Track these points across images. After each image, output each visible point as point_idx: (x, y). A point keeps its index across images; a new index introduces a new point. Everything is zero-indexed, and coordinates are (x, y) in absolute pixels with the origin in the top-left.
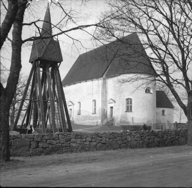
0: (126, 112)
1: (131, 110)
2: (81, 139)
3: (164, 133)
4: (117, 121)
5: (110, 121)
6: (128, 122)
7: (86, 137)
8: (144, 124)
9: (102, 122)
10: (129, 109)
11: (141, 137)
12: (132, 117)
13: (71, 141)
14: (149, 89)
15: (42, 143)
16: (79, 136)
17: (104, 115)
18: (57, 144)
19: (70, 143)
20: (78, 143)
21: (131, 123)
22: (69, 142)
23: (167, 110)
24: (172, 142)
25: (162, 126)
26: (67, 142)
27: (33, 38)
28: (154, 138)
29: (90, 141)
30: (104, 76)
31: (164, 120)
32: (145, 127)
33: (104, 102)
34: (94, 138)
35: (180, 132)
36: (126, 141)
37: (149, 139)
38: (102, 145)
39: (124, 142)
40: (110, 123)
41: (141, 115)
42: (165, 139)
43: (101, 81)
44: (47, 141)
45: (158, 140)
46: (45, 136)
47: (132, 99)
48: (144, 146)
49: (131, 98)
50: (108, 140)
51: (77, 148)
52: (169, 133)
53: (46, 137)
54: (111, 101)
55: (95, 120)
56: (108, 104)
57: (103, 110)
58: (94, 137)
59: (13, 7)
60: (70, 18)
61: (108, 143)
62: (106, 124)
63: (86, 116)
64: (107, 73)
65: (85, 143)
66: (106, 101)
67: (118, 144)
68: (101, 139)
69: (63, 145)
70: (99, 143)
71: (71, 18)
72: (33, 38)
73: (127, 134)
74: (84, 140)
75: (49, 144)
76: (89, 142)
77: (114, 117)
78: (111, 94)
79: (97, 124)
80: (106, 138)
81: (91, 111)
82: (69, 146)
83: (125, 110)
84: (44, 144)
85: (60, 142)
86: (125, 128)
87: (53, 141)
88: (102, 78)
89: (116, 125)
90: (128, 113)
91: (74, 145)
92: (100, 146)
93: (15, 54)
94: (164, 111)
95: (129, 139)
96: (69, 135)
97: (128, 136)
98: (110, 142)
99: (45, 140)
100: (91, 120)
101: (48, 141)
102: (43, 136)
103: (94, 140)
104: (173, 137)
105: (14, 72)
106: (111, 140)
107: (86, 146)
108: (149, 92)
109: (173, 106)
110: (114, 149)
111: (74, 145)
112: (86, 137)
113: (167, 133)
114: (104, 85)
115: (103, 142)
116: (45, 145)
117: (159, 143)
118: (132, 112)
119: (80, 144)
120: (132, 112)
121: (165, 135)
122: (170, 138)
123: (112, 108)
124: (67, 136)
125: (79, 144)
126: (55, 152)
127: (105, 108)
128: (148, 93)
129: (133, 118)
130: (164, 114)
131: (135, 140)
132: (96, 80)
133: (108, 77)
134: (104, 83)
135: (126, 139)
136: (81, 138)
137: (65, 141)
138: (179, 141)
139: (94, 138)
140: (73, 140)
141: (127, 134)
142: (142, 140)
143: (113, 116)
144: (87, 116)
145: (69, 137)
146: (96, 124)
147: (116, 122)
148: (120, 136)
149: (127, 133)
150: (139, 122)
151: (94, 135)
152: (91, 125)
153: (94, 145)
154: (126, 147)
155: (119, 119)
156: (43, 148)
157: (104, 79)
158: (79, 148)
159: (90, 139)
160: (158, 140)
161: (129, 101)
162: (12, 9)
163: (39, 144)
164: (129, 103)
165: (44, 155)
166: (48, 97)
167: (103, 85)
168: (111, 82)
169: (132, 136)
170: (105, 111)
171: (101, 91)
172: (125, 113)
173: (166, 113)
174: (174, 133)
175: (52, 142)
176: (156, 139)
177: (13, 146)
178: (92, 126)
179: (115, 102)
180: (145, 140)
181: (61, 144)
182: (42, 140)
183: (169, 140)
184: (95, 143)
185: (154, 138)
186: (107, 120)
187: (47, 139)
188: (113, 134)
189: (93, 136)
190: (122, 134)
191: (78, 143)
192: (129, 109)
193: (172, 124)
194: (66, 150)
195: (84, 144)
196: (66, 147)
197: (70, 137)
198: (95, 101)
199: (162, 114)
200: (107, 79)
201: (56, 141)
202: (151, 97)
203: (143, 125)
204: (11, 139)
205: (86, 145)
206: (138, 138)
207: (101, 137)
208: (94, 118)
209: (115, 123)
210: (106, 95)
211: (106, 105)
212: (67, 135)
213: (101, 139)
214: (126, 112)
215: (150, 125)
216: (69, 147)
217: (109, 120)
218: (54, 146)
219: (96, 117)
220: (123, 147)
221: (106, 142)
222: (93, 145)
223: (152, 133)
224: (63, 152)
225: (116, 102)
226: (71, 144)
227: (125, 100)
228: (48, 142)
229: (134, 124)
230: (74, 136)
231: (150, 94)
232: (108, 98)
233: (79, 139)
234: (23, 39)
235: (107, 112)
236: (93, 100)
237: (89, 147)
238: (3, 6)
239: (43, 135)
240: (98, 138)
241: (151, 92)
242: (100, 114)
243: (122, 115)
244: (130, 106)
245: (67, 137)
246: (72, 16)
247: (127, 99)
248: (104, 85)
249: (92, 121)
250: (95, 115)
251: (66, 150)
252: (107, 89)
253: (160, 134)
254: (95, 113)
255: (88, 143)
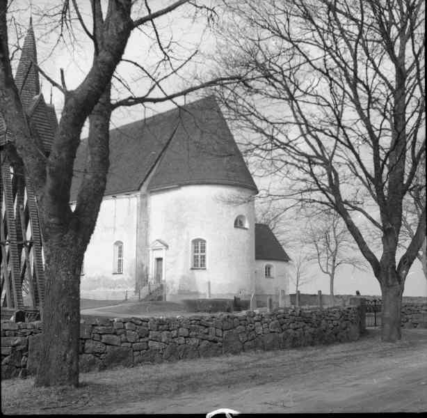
0: (192, 269)
1: (203, 265)
2: (168, 332)
3: (320, 316)
4: (171, 290)
5: (157, 290)
6: (197, 293)
7: (179, 328)
8: (235, 297)
9: (136, 292)
10: (199, 262)
11: (282, 325)
12: (207, 280)
13: (150, 337)
14: (241, 220)
15: (92, 341)
16: (165, 326)
17: (142, 278)
18: (122, 345)
19: (147, 342)
20: (163, 340)
21: (205, 294)
22: (146, 339)
23: (276, 266)
24: (336, 335)
25: (271, 300)
26: (141, 340)
27: (130, 101)
28: (304, 326)
29: (186, 335)
30: (144, 189)
31: (270, 287)
32: (238, 304)
33: (143, 246)
34: (195, 329)
35: (348, 312)
36: (253, 334)
37: (295, 329)
38: (210, 343)
39: (250, 338)
40: (156, 298)
41: (222, 277)
42: (324, 327)
43: (136, 198)
44: (101, 338)
45: (312, 330)
46: (96, 325)
47: (205, 241)
48: (288, 345)
49: (205, 239)
50: (219, 332)
51: (161, 352)
52: (331, 314)
53: (100, 328)
54: (159, 245)
55: (119, 287)
56: (151, 252)
57: (140, 266)
58: (193, 326)
59: (124, 27)
60: (167, 58)
61: (221, 339)
62: (147, 296)
63: (96, 279)
64: (151, 181)
65: (175, 340)
66: (147, 245)
67: (239, 342)
68: (206, 331)
69: (134, 345)
70: (203, 340)
71: (169, 59)
72: (130, 101)
73: (255, 318)
74: (174, 333)
75: (106, 344)
76: (185, 337)
77: (165, 281)
78: (157, 231)
79: (126, 297)
80: (216, 328)
81: (111, 266)
82: (146, 348)
83: (190, 265)
84: (96, 344)
85: (129, 340)
86: (194, 305)
87: (115, 336)
88: (139, 194)
89: (168, 299)
90: (195, 271)
91: (156, 345)
92: (207, 348)
93: (99, 136)
94: (269, 268)
95: (260, 330)
96: (144, 323)
97: (256, 323)
98: (225, 338)
99: (98, 336)
100: (111, 288)
101: (103, 336)
102: (93, 325)
103: (195, 333)
104: (338, 325)
105: (97, 176)
106: (226, 332)
107: (178, 349)
108: (242, 225)
109: (288, 257)
110: (235, 353)
111: (156, 345)
112: (179, 328)
113: (325, 315)
114: (143, 208)
115: (211, 337)
116: (98, 347)
117: (313, 338)
118: (205, 269)
119: (168, 344)
120: (205, 269)
121: (323, 321)
122: (331, 326)
123: (159, 260)
124: (141, 325)
125: (164, 343)
126: (119, 361)
127: (144, 262)
128: (239, 228)
129: (209, 283)
130: (269, 275)
131: (271, 332)
132: (124, 196)
133: (151, 192)
134: (142, 204)
135: (253, 330)
136: (168, 330)
137: (138, 337)
138: (347, 332)
139: (195, 329)
140: (153, 334)
141: (255, 318)
142: (283, 330)
143: (163, 278)
144: (99, 279)
145: (146, 328)
146: (124, 298)
147: (170, 293)
148: (242, 322)
149: (254, 316)
150: (220, 292)
151: (193, 322)
152: (110, 299)
153: (194, 345)
154: (254, 348)
155: (176, 286)
156: (94, 353)
157: (144, 196)
158: (166, 353)
159: (186, 332)
160: (312, 330)
161: (199, 245)
162: (119, 31)
163: (86, 344)
164: (200, 250)
165: (97, 369)
166: (6, 234)
167: (142, 207)
168: (159, 202)
169: (265, 323)
170: (144, 268)
171: (135, 223)
172: (191, 272)
173: (273, 272)
174: (337, 315)
175: (113, 340)
176: (309, 330)
177: (32, 350)
178: (115, 303)
179: (167, 247)
180: (289, 331)
181: (130, 344)
182: (92, 335)
183: (330, 331)
184: (195, 341)
185: (304, 326)
186: (149, 289)
187: (101, 332)
188: (229, 320)
189: (191, 324)
190: (246, 320)
191: (163, 340)
192: (199, 262)
193: (287, 296)
194: (140, 358)
195: (175, 342)
196: (140, 351)
197: (147, 326)
198: (119, 244)
199: (266, 275)
200: (148, 195)
201: (121, 337)
202: (245, 238)
203: (233, 298)
204: (27, 334)
205: (179, 345)
206: (275, 328)
207: (207, 327)
208: (115, 285)
209: (165, 295)
210: (147, 232)
211: (146, 255)
212: (140, 322)
213: (206, 331)
214: (192, 269)
215: (247, 299)
216: (147, 350)
217: (153, 288)
218: (116, 348)
219: (122, 281)
220: (250, 348)
221: (217, 338)
222: (192, 344)
223: (300, 315)
224: (135, 361)
225: (170, 248)
226: (149, 344)
227: (190, 242)
228: (103, 341)
229: (212, 298)
230: (155, 326)
231: (243, 231)
232: (152, 238)
233: (165, 332)
234: (113, 102)
235: (147, 269)
236: (115, 241)
237: (185, 349)
238: (78, 21)
239: (94, 323)
240: (201, 329)
241: (247, 225)
242: (131, 275)
243: (183, 277)
244: (201, 256)
245: (142, 327)
246: (170, 54)
247: (195, 242)
248: (143, 208)
249: (112, 290)
250: (119, 277)
251: (140, 358)
252: (148, 217)
253: (314, 317)
254: (120, 272)
255: (182, 340)
